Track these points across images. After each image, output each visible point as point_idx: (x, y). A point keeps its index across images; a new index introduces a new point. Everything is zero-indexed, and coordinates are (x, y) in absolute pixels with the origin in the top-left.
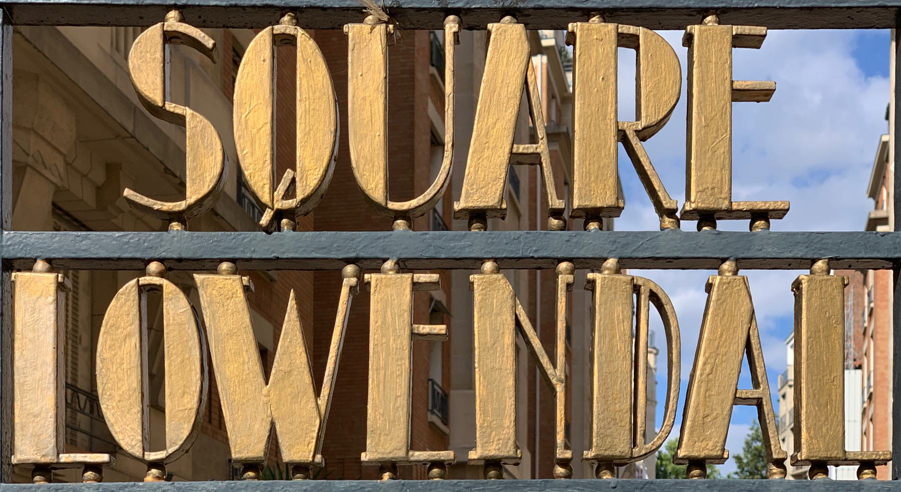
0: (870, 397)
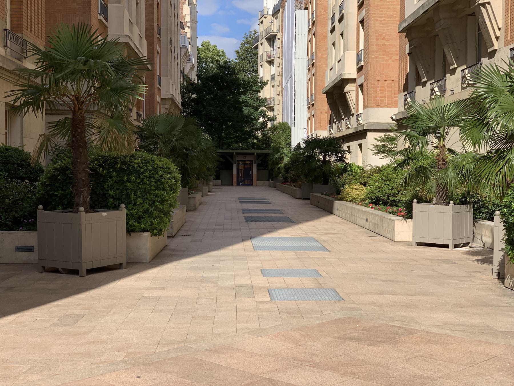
0: (313, 24)
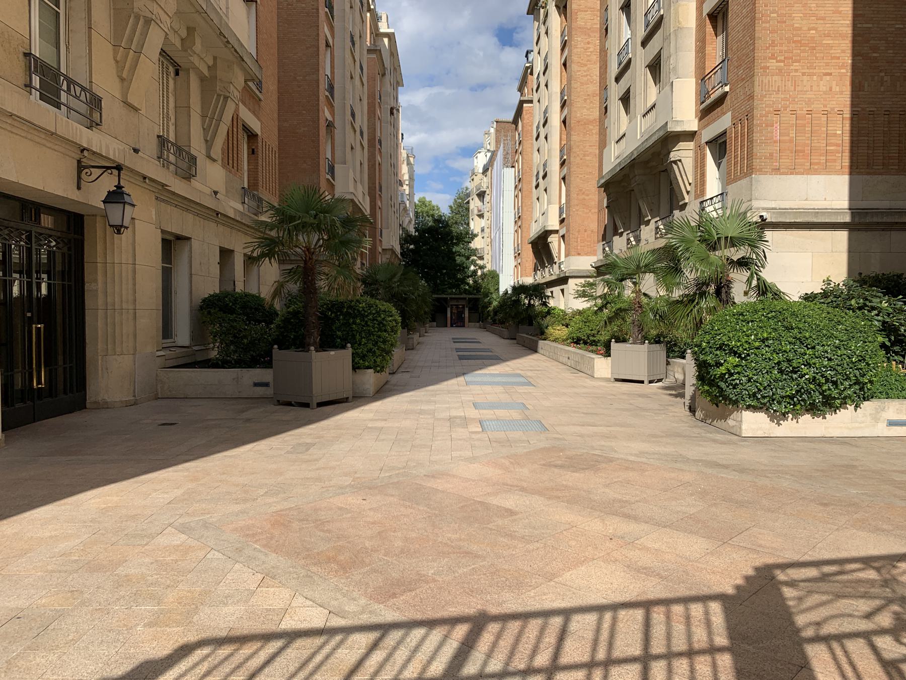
0: (519, 181)
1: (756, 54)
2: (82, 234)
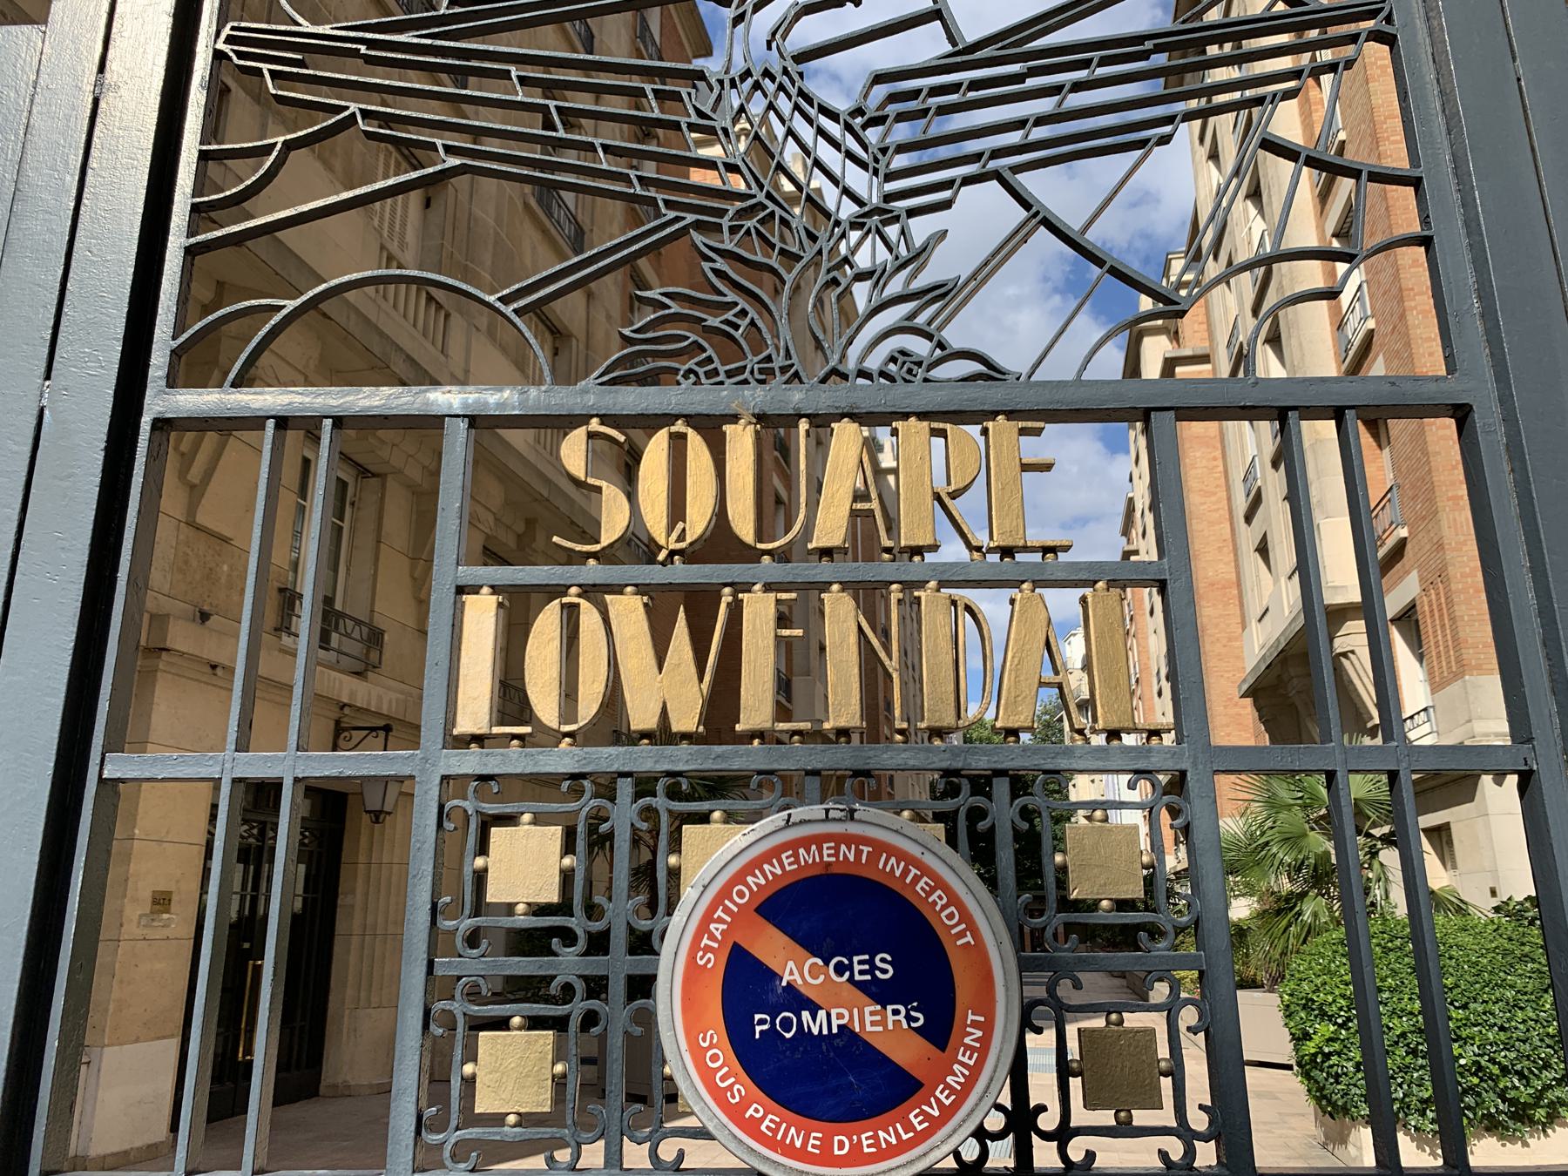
1: (1434, 479)
2: (343, 821)
